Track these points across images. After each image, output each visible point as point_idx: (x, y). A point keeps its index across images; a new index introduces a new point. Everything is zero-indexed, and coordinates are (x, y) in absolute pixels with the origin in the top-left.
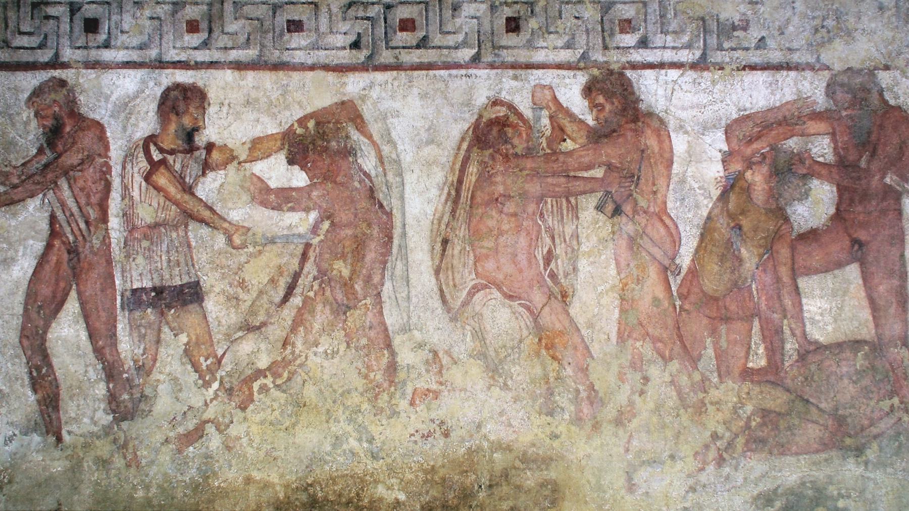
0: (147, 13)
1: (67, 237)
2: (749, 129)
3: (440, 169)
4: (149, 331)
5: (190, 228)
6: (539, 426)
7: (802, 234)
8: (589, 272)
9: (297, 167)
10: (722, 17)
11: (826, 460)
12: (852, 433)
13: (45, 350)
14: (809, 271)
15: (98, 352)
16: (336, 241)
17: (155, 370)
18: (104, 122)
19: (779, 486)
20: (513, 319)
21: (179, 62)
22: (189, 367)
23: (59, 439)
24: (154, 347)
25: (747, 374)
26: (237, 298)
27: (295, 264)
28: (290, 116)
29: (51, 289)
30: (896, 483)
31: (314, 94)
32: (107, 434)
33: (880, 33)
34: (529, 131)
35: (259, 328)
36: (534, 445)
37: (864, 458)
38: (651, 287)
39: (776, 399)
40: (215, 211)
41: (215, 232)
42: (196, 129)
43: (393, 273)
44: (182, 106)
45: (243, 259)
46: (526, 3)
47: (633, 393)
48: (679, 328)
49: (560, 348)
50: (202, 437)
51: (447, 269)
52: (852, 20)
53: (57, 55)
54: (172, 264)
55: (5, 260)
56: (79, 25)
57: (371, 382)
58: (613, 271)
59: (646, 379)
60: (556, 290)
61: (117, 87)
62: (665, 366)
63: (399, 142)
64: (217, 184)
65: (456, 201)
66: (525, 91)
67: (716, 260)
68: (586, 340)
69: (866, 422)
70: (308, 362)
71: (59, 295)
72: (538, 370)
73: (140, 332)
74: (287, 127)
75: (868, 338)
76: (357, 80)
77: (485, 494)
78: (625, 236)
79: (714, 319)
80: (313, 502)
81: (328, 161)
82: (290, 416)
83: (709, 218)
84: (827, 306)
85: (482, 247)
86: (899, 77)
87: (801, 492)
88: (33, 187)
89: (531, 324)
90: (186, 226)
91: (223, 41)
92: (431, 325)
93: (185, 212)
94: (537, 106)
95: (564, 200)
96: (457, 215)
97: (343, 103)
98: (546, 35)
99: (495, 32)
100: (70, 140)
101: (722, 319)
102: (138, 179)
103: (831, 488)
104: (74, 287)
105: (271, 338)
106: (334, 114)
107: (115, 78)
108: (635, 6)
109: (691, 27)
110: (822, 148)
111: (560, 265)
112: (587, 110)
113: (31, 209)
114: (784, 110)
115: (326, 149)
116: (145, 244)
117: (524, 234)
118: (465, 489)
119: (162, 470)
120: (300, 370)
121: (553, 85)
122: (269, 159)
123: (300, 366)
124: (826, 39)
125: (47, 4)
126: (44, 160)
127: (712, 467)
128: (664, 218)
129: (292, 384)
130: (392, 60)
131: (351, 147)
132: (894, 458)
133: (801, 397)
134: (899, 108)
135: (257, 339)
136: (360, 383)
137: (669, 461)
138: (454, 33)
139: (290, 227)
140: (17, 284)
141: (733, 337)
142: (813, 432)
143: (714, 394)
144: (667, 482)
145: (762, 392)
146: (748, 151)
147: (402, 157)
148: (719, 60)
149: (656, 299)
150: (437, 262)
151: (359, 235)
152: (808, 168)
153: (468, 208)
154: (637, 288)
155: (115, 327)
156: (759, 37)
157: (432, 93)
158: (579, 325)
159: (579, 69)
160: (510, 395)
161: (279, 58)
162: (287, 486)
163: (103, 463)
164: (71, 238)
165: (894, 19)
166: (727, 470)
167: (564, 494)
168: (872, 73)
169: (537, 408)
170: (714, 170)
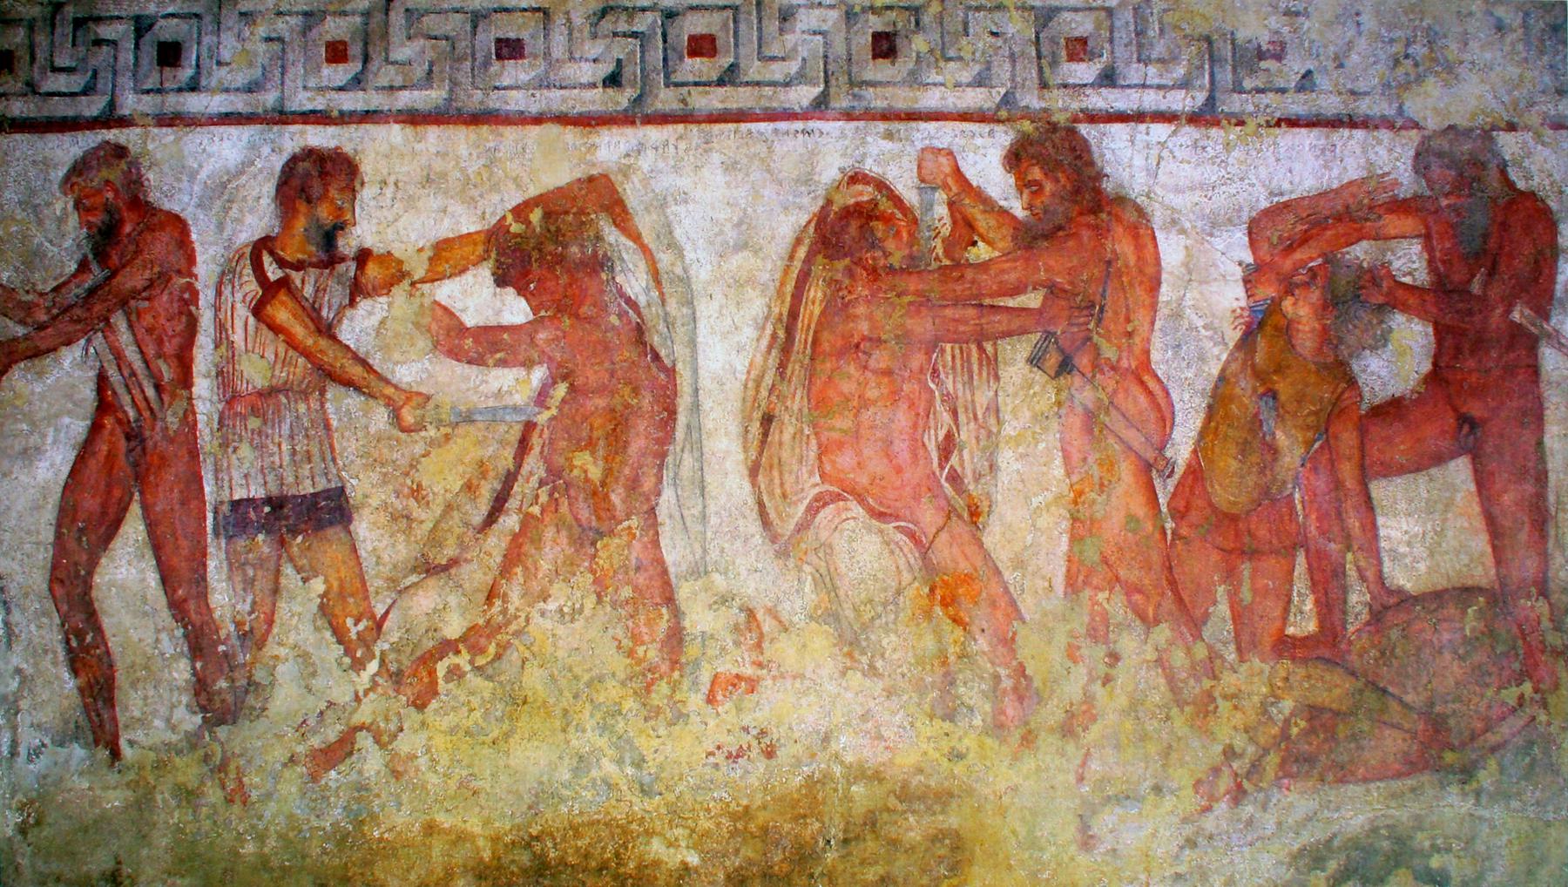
0: (262, 30)
1: (125, 412)
2: (1289, 226)
3: (758, 292)
4: (260, 573)
5: (329, 395)
6: (929, 739)
7: (1378, 407)
8: (1018, 471)
9: (510, 290)
10: (1241, 36)
11: (1413, 790)
12: (1456, 743)
13: (90, 603)
14: (1389, 470)
15: (177, 608)
16: (578, 419)
17: (270, 639)
18: (187, 215)
19: (1335, 835)
20: (886, 553)
21: (313, 112)
22: (328, 634)
23: (116, 754)
24: (268, 601)
25: (1285, 646)
26: (407, 517)
27: (507, 459)
28: (500, 203)
29: (98, 500)
30: (1525, 826)
31: (543, 163)
32: (193, 747)
33: (1499, 69)
34: (913, 227)
35: (446, 568)
36: (920, 771)
37: (1475, 785)
38: (1121, 502)
39: (1331, 688)
40: (371, 367)
41: (371, 401)
42: (340, 227)
43: (676, 474)
44: (316, 189)
45: (419, 449)
46: (907, 9)
47: (1092, 680)
48: (1170, 568)
49: (966, 603)
50: (351, 753)
51: (771, 467)
52: (1454, 46)
53: (112, 105)
54: (298, 458)
55: (25, 450)
56: (149, 53)
57: (639, 662)
58: (1058, 470)
59: (1115, 657)
60: (960, 503)
61: (210, 156)
62: (1147, 633)
63: (688, 247)
64: (374, 321)
65: (786, 350)
66: (905, 159)
67: (1233, 450)
68: (1012, 589)
69: (1479, 725)
70: (530, 628)
71: (112, 510)
72: (929, 643)
73: (245, 574)
74: (494, 221)
75: (1484, 583)
76: (615, 140)
77: (836, 855)
78: (1080, 410)
79: (1231, 552)
80: (541, 867)
81: (564, 280)
82: (500, 720)
83: (1223, 377)
84: (1417, 529)
85: (832, 429)
86: (1531, 143)
87: (1371, 845)
88: (71, 328)
89: (916, 563)
90: (323, 392)
91: (388, 75)
92: (743, 564)
93: (320, 368)
94: (925, 182)
95: (974, 347)
96: (789, 372)
97: (591, 179)
98: (942, 64)
99: (854, 58)
100: (132, 248)
101: (1243, 552)
102: (242, 312)
103: (1419, 836)
104: (137, 496)
105: (467, 586)
106: (574, 199)
107: (205, 142)
108: (1094, 15)
109: (1189, 53)
110: (1409, 261)
111: (968, 459)
112: (1013, 191)
113: (66, 364)
114: (1345, 194)
115: (560, 259)
116: (254, 423)
117: (905, 407)
118: (801, 847)
119: (285, 809)
120: (516, 642)
121: (955, 149)
122: (464, 277)
123: (518, 634)
124: (1412, 78)
125: (99, 20)
126: (89, 282)
127: (1224, 805)
128: (1146, 378)
129: (503, 665)
130: (675, 106)
131: (605, 255)
132: (1523, 783)
133: (1373, 684)
134: (1531, 195)
135: (442, 588)
136: (620, 664)
137: (1152, 797)
138: (783, 59)
139: (499, 394)
140: (45, 491)
141: (1263, 582)
142: (1393, 743)
143: (1229, 681)
144: (1148, 832)
145: (1309, 677)
146: (1288, 264)
147: (692, 272)
148: (1236, 108)
149: (1131, 518)
150: (753, 454)
151: (619, 408)
152: (1388, 295)
153: (807, 361)
154: (1100, 499)
155: (205, 565)
156: (1303, 71)
157: (745, 161)
158: (1000, 565)
159: (999, 121)
160: (881, 685)
161: (481, 103)
162: (495, 840)
163: (188, 796)
164: (132, 414)
165: (1520, 47)
166: (1248, 809)
167: (972, 853)
168: (1487, 134)
169: (927, 707)
170: (1230, 297)
